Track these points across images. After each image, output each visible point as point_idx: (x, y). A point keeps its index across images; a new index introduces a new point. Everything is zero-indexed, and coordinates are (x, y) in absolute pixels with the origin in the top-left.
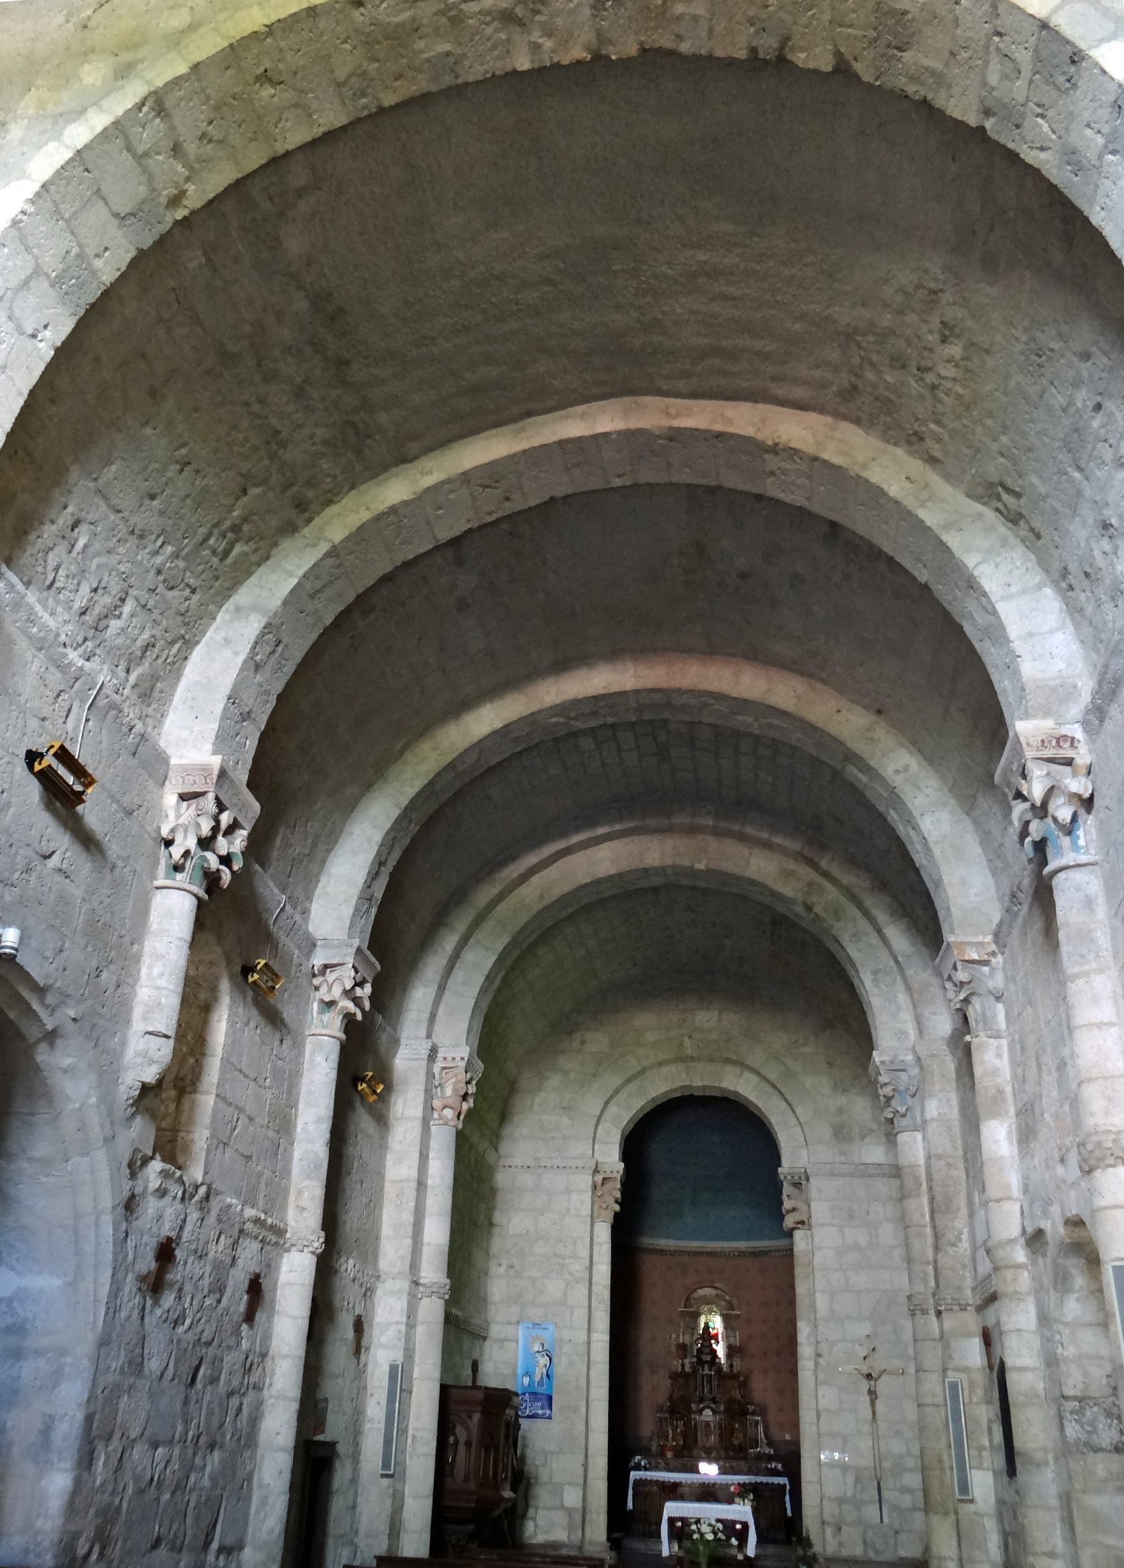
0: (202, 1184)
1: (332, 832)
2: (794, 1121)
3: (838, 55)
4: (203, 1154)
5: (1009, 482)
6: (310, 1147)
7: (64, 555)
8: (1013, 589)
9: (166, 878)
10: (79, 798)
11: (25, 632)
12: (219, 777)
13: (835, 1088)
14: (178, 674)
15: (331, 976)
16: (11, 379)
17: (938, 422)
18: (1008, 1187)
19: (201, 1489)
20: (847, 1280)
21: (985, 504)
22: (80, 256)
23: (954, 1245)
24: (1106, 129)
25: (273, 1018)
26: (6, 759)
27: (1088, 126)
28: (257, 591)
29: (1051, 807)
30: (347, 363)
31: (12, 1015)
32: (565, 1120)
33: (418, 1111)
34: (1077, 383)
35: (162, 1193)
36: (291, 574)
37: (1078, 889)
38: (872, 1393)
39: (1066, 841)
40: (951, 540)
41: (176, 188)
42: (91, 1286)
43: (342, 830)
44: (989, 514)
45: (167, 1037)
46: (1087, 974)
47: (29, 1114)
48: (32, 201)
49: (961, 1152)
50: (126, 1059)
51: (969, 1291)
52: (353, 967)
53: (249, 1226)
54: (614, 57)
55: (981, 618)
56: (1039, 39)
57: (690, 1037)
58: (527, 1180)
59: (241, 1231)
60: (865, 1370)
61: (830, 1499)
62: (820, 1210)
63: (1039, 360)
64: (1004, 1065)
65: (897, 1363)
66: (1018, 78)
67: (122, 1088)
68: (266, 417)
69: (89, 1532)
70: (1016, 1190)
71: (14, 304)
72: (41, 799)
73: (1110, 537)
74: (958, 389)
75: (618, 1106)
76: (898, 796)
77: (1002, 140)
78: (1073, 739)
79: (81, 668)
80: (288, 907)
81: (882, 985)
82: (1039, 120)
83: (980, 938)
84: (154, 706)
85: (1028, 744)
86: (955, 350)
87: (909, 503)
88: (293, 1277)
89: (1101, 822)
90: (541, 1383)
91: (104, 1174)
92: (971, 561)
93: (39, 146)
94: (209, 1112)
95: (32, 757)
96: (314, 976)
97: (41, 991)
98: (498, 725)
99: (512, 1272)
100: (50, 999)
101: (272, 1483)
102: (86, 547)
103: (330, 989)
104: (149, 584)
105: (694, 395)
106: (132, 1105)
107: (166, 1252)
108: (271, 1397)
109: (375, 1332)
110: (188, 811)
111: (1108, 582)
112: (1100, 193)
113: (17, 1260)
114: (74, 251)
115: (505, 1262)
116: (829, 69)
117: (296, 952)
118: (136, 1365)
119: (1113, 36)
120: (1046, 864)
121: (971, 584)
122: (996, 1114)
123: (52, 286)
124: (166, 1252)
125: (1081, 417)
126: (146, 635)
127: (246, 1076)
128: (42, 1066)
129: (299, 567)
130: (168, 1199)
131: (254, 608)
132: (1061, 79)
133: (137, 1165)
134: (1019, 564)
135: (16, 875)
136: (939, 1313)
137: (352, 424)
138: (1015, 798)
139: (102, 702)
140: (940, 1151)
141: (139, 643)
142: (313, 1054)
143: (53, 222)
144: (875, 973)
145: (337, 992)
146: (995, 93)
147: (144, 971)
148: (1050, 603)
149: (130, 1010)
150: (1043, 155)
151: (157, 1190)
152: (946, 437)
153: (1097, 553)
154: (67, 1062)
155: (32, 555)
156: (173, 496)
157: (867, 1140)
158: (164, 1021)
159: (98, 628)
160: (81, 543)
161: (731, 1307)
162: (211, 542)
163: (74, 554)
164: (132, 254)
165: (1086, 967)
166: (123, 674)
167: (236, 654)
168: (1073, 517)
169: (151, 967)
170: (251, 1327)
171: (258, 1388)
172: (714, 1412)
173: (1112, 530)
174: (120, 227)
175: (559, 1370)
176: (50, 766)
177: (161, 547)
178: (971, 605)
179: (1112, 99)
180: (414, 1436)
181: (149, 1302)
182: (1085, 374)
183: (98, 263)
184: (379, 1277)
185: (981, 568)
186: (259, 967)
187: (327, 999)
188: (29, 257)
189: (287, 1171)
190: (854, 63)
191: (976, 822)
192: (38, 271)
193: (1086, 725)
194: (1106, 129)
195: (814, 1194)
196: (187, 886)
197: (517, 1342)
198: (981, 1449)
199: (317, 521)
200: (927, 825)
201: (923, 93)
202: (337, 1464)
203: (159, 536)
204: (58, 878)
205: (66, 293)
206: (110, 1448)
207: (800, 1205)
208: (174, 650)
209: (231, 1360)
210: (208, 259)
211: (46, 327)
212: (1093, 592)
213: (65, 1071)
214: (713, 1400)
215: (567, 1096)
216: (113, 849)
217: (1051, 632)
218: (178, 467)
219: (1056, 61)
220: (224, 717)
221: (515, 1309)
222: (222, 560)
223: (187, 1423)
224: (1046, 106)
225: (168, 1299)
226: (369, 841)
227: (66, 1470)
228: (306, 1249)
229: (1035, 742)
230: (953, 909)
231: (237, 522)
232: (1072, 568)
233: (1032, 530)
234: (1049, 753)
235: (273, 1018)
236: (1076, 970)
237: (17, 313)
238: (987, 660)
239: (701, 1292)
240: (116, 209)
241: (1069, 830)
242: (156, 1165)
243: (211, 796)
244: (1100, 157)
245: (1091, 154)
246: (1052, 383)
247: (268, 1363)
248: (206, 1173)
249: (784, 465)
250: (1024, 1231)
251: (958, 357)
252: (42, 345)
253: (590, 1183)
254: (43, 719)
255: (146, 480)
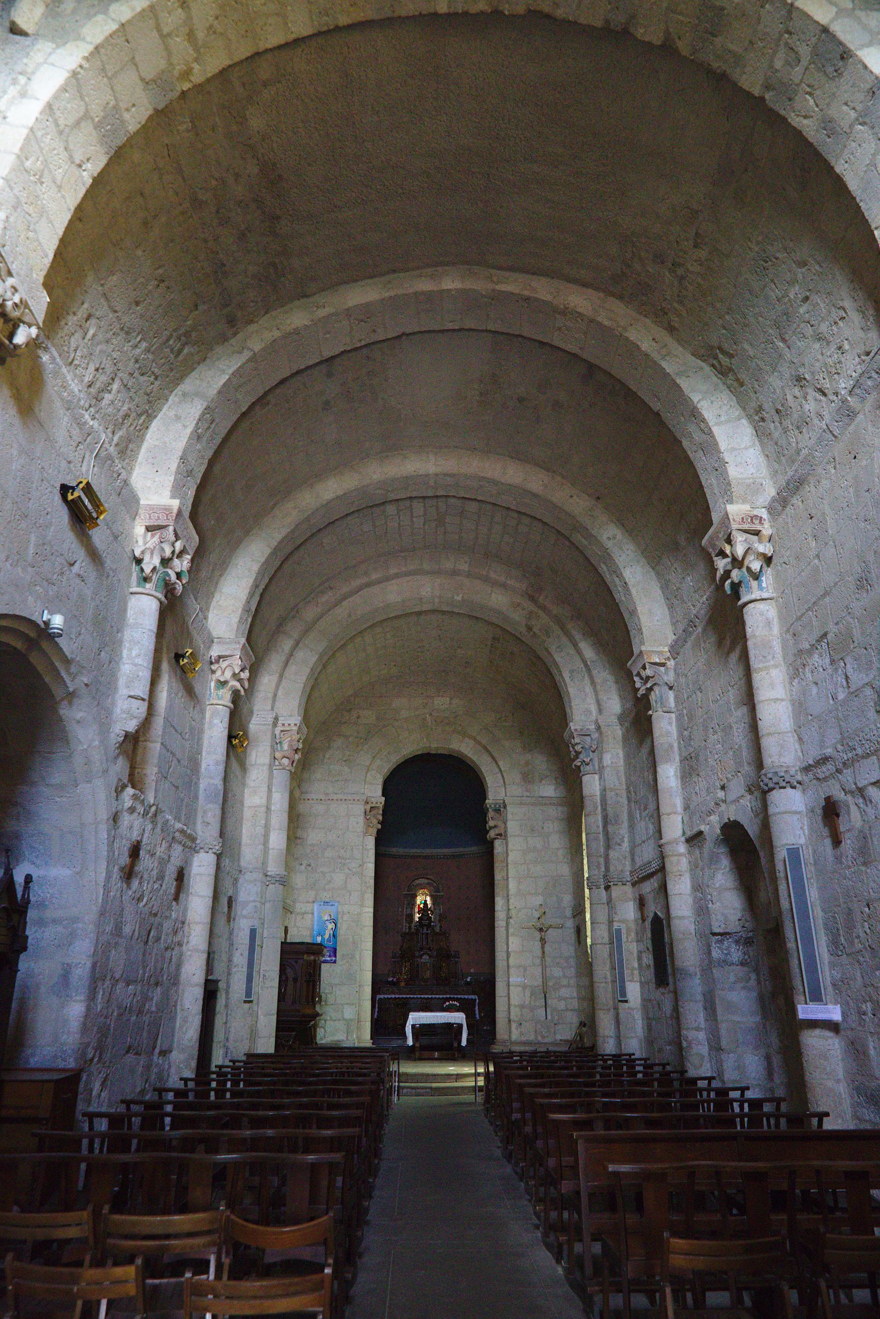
0: (154, 805)
1: (224, 563)
2: (497, 770)
3: (667, 33)
4: (154, 784)
5: (725, 346)
6: (212, 781)
7: (80, 339)
8: (723, 419)
9: (139, 585)
10: (94, 522)
11: (60, 396)
12: (177, 515)
13: (524, 748)
14: (141, 438)
15: (223, 664)
16: (63, 197)
17: (681, 303)
18: (675, 806)
19: (152, 1013)
20: (529, 870)
21: (704, 361)
22: (116, 108)
23: (619, 845)
24: (859, 107)
25: (190, 691)
26: (49, 489)
27: (846, 104)
28: (198, 382)
29: (746, 563)
30: (278, 218)
31: (47, 679)
32: (346, 769)
33: (267, 760)
34: (791, 283)
35: (132, 810)
36: (223, 372)
37: (761, 614)
38: (543, 941)
39: (754, 584)
40: (682, 382)
41: (186, 65)
42: (93, 874)
43: (229, 562)
44: (707, 369)
45: (143, 700)
46: (767, 668)
47: (49, 753)
48: (87, 59)
49: (624, 787)
50: (115, 715)
51: (628, 873)
52: (240, 658)
53: (177, 834)
54: (507, 13)
55: (697, 436)
56: (819, 39)
57: (431, 715)
58: (320, 808)
59: (173, 838)
60: (539, 925)
61: (515, 1006)
62: (513, 826)
63: (765, 265)
64: (674, 730)
65: (559, 921)
66: (797, 65)
67: (112, 735)
68: (217, 253)
69: (94, 1043)
70: (679, 807)
71: (70, 139)
72: (69, 523)
73: (802, 387)
74: (699, 280)
75: (381, 760)
76: (609, 554)
77: (776, 108)
78: (761, 518)
79: (92, 427)
80: (200, 614)
81: (576, 680)
82: (807, 96)
83: (661, 649)
84: (127, 461)
85: (734, 520)
86: (703, 254)
87: (655, 356)
88: (202, 870)
89: (778, 572)
90: (329, 940)
91: (102, 795)
92: (695, 398)
93: (89, 17)
94: (157, 755)
95: (65, 489)
96: (211, 663)
97: (67, 661)
98: (340, 492)
99: (310, 868)
100: (73, 669)
101: (190, 1007)
102: (94, 336)
103: (223, 673)
104: (130, 369)
105: (512, 269)
106: (118, 748)
107: (135, 851)
108: (188, 950)
109: (239, 908)
110: (153, 540)
111: (795, 416)
112: (846, 151)
113: (37, 857)
114: (112, 103)
115: (305, 862)
116: (659, 43)
117: (202, 646)
118: (118, 931)
119: (870, 44)
120: (739, 599)
121: (695, 414)
122: (668, 760)
123: (95, 128)
124: (135, 851)
125: (792, 306)
126: (125, 408)
127: (176, 731)
128: (64, 718)
129: (229, 367)
130: (135, 814)
131: (197, 394)
132: (831, 69)
133: (119, 790)
134: (725, 402)
135: (55, 577)
136: (607, 888)
137: (274, 265)
138: (717, 555)
139: (103, 454)
140: (612, 786)
141: (121, 413)
142: (212, 717)
143: (100, 77)
144: (572, 671)
145: (228, 675)
146: (778, 75)
147: (125, 653)
148: (745, 431)
149: (117, 679)
150: (805, 122)
151: (129, 808)
152: (684, 314)
153: (789, 398)
154: (79, 715)
155: (62, 337)
156: (150, 304)
157: (543, 782)
158: (141, 688)
159: (99, 400)
160: (91, 332)
161: (438, 891)
162: (171, 342)
163: (86, 341)
164: (150, 112)
165: (767, 664)
166: (110, 435)
167: (185, 426)
168: (773, 373)
169: (130, 649)
170: (178, 904)
171: (180, 944)
172: (430, 956)
173: (804, 382)
174: (144, 90)
175: (342, 931)
176: (79, 497)
177: (140, 342)
178: (692, 428)
179: (868, 86)
180: (264, 976)
181: (125, 886)
182: (800, 276)
183: (127, 116)
184: (240, 871)
185: (702, 403)
186: (187, 654)
187: (222, 680)
188: (82, 103)
189: (196, 797)
190: (677, 41)
191: (658, 574)
192: (86, 116)
193: (770, 509)
194: (859, 107)
195: (509, 816)
196: (154, 593)
197: (313, 914)
198: (633, 969)
199: (240, 336)
200: (627, 574)
201: (724, 68)
202: (219, 993)
203: (139, 334)
204: (78, 581)
205: (104, 136)
206: (105, 986)
207: (500, 823)
208: (141, 421)
209: (167, 925)
210: (194, 126)
211: (88, 160)
212: (781, 423)
213: (78, 722)
214: (429, 949)
215: (348, 753)
216: (108, 563)
217: (746, 448)
218: (156, 283)
219: (828, 56)
220: (177, 472)
221: (312, 894)
222: (176, 357)
223: (144, 968)
224: (816, 87)
225: (135, 883)
226: (249, 570)
227: (81, 1001)
228: (210, 851)
229: (738, 519)
230: (644, 630)
231: (188, 329)
232: (766, 406)
233: (737, 380)
234: (746, 526)
235: (190, 691)
236: (761, 665)
237: (71, 146)
238: (698, 466)
239: (417, 882)
240: (143, 75)
241: (756, 577)
242: (130, 791)
243: (171, 528)
244: (851, 126)
245: (845, 124)
246: (772, 281)
247: (186, 928)
248: (155, 797)
249: (569, 323)
250: (684, 833)
251: (703, 259)
252: (85, 173)
253: (363, 810)
254: (69, 462)
255: (135, 290)
